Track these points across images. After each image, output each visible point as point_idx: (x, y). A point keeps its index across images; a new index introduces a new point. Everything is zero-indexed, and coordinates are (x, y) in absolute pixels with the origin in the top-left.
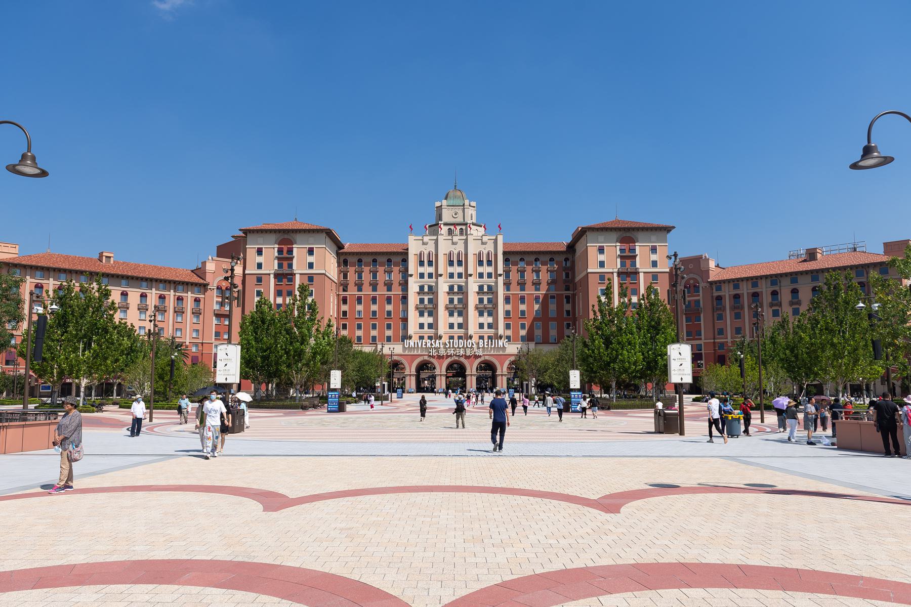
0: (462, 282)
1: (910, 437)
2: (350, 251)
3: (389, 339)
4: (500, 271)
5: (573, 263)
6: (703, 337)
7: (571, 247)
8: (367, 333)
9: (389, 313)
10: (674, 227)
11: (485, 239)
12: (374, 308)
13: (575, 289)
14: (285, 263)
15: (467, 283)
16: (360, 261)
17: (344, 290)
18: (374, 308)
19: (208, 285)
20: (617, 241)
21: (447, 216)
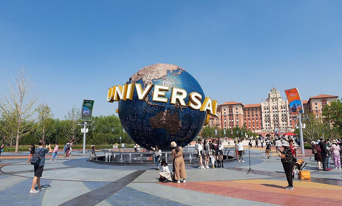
0: (277, 113)
3: (258, 129)
4: (288, 110)
8: (256, 127)
9: (257, 122)
11: (283, 102)
12: (253, 121)
14: (231, 112)
15: (278, 114)
16: (249, 109)
17: (245, 117)
18: (253, 121)
21: (271, 96)
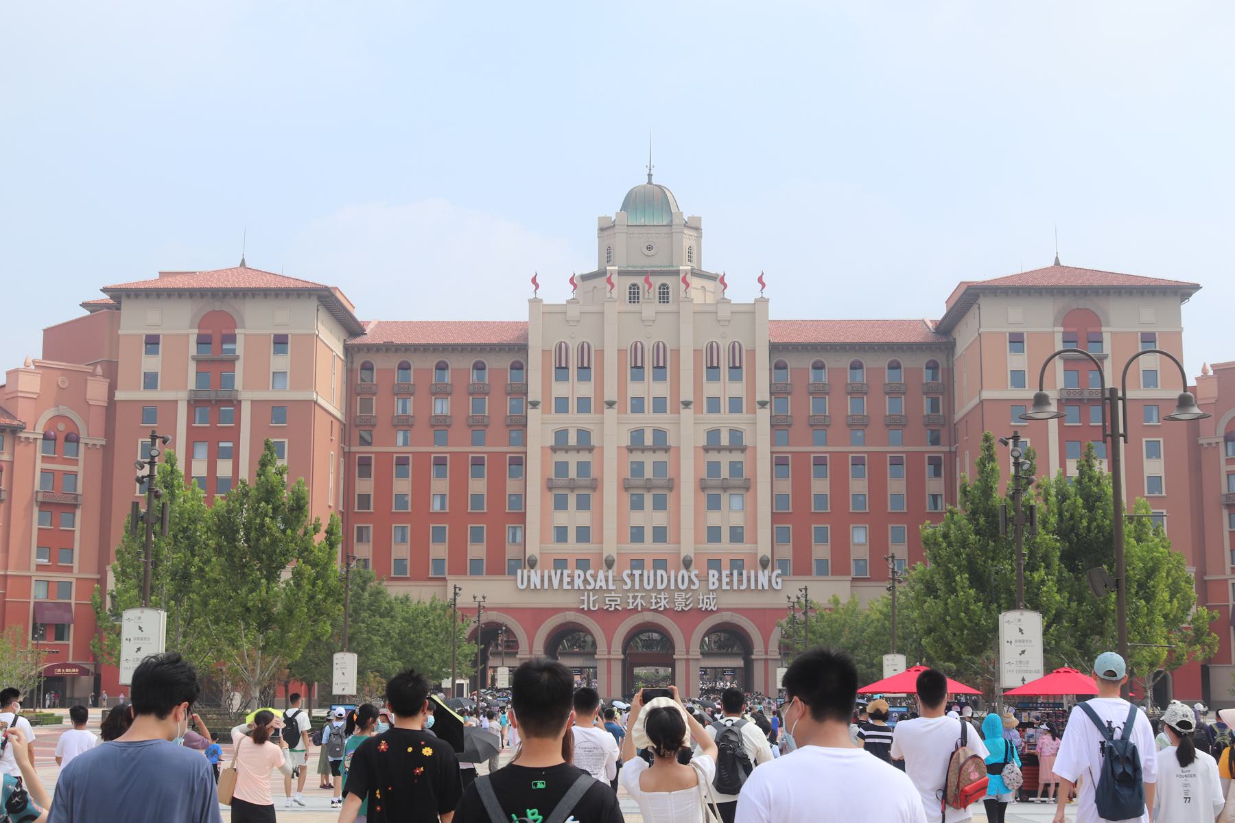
1: (953, 816)
2: (379, 340)
4: (763, 393)
5: (950, 372)
6: (76, 565)
7: (946, 329)
10: (1197, 287)
13: (953, 440)
17: (364, 442)
19: (22, 428)
20: (191, 327)
